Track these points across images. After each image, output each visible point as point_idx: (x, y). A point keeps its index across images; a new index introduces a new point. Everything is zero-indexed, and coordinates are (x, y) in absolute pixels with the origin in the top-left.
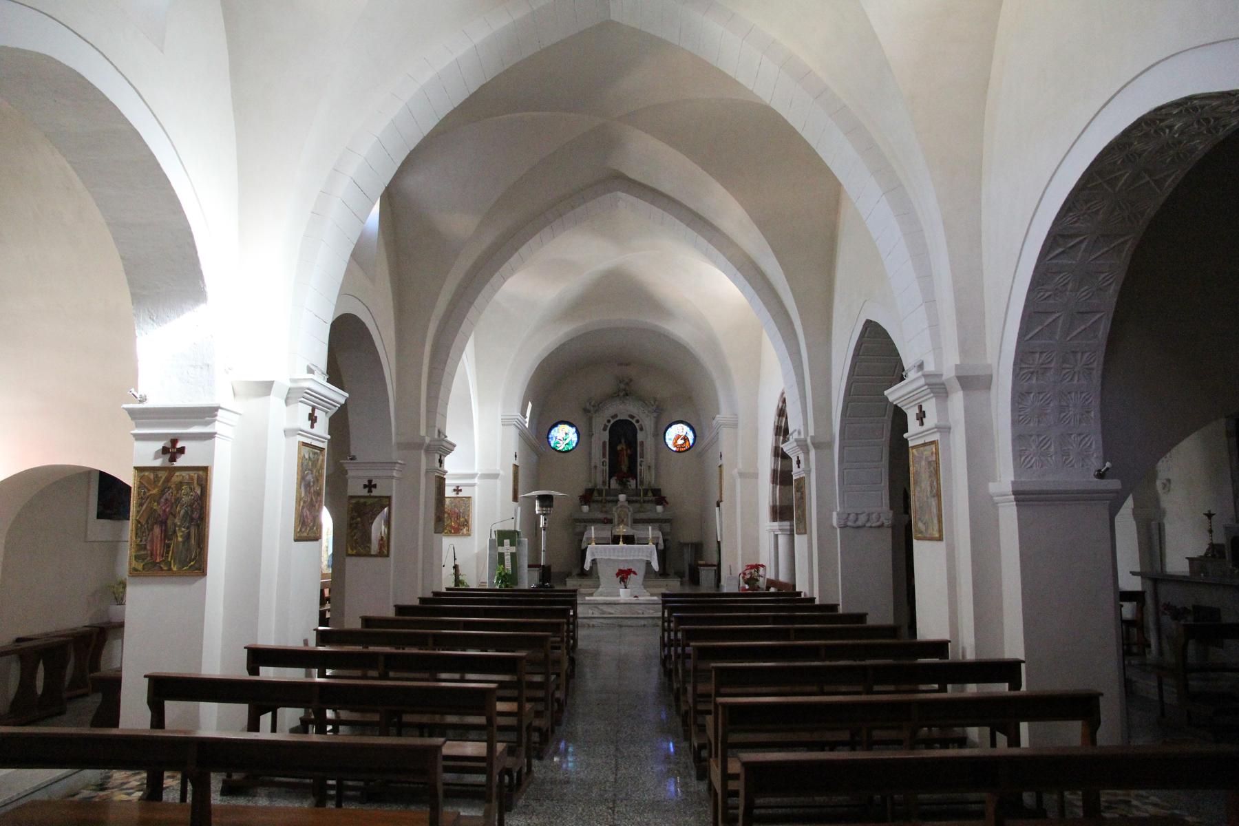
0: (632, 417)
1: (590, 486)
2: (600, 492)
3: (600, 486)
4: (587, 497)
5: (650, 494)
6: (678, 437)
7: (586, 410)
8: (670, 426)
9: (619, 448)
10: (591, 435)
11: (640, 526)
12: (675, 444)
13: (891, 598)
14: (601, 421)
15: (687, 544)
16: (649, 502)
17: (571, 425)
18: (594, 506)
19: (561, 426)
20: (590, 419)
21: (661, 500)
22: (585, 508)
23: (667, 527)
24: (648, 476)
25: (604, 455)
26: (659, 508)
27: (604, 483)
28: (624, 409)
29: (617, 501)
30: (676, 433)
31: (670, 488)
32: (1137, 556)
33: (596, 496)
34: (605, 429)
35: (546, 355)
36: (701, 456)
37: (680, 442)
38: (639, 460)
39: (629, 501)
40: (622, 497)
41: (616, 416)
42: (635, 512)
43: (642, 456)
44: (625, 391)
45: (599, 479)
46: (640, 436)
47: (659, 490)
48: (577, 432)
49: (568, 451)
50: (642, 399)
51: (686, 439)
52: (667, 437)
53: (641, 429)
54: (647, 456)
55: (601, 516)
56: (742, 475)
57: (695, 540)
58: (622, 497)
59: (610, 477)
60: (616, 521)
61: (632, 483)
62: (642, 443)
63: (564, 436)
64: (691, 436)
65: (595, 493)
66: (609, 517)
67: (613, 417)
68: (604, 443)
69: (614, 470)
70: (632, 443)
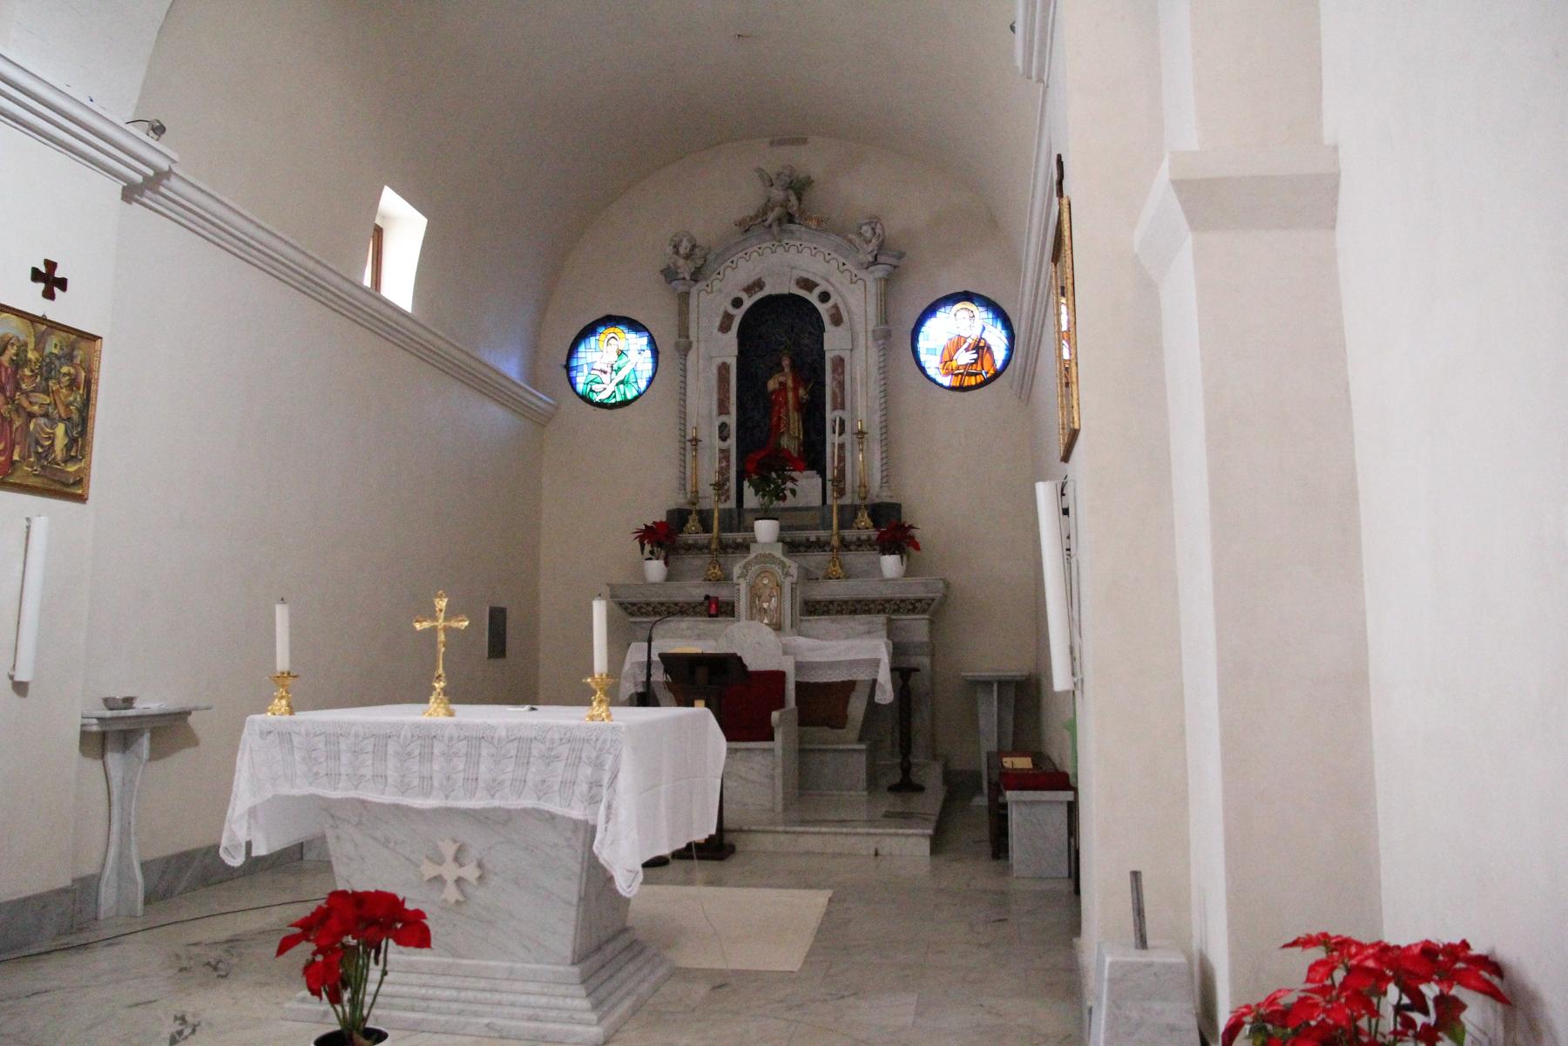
0: (808, 285)
3: (709, 500)
4: (662, 537)
5: (864, 520)
6: (957, 343)
7: (669, 274)
8: (931, 311)
10: (684, 349)
11: (822, 623)
12: (947, 360)
14: (715, 302)
15: (986, 684)
16: (860, 544)
18: (697, 562)
19: (605, 334)
20: (684, 298)
21: (893, 530)
22: (655, 569)
23: (917, 628)
24: (864, 468)
25: (723, 408)
26: (890, 564)
27: (720, 486)
28: (781, 266)
29: (1349, 970)
30: (952, 333)
31: (937, 497)
33: (692, 533)
34: (724, 328)
35: (1044, 701)
36: (1026, 390)
37: (964, 358)
39: (792, 547)
40: (765, 530)
41: (759, 284)
42: (808, 576)
43: (840, 405)
44: (790, 208)
46: (834, 341)
47: (896, 508)
48: (652, 342)
49: (625, 403)
50: (824, 226)
51: (981, 348)
52: (922, 345)
53: (837, 320)
54: (858, 399)
55: (694, 590)
56: (1207, 200)
57: (1014, 667)
58: (765, 530)
60: (742, 605)
61: (807, 488)
62: (839, 362)
63: (616, 362)
64: (997, 339)
65: (693, 524)
66: (723, 593)
67: (749, 290)
68: (723, 369)
70: (811, 368)
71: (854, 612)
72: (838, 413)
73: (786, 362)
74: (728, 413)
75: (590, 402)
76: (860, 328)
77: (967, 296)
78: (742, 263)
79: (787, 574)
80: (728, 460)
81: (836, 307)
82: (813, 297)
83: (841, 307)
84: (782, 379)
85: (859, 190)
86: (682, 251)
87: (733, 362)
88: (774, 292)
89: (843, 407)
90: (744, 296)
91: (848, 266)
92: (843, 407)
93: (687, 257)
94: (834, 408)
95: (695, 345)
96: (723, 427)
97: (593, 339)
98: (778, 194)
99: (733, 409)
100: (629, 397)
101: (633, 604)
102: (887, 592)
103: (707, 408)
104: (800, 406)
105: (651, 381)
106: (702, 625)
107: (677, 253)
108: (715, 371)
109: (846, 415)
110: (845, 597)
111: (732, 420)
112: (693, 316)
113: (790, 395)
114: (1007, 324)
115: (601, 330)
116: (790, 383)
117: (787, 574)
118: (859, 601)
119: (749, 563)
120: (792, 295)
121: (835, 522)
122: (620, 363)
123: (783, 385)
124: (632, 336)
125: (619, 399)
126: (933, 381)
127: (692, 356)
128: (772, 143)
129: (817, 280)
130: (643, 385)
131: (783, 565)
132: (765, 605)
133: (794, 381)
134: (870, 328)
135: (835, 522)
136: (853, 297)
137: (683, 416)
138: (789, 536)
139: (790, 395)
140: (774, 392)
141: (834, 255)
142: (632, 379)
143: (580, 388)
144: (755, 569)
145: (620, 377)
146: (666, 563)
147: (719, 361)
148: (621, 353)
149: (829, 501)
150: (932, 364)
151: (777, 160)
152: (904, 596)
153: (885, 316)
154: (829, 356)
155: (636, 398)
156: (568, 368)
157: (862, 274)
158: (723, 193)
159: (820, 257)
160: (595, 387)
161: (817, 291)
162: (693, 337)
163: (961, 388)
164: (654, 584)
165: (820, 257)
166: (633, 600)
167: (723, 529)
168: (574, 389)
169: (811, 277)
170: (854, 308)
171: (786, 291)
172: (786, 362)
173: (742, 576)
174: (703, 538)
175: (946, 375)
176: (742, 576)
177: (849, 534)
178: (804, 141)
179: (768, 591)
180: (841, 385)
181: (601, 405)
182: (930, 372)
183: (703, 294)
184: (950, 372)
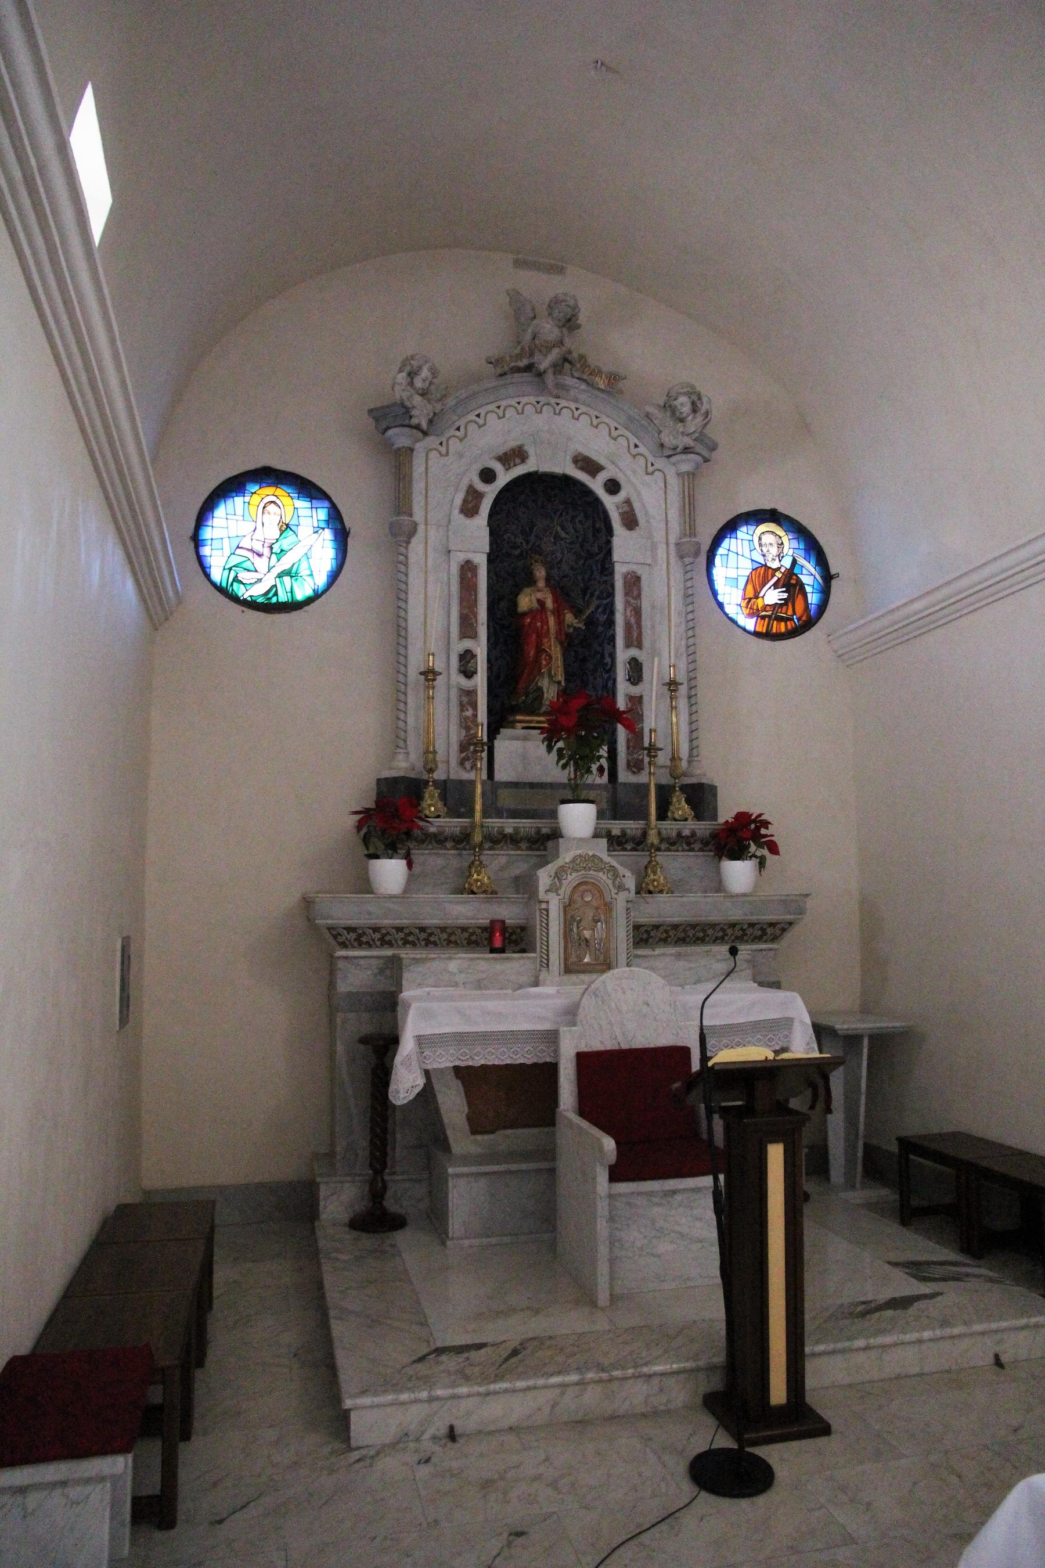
0: (592, 467)
1: (403, 766)
2: (457, 799)
3: (449, 767)
4: (392, 817)
5: (681, 807)
6: (762, 575)
9: (526, 601)
10: (400, 532)
12: (750, 601)
13: (74, 1258)
14: (449, 474)
16: (673, 843)
17: (307, 489)
18: (430, 859)
19: (258, 495)
20: (399, 463)
22: (390, 873)
25: (467, 628)
26: (739, 873)
27: (468, 747)
28: (559, 435)
32: (1014, 1141)
34: (469, 509)
37: (772, 596)
38: (622, 655)
43: (635, 640)
44: (544, 359)
45: (447, 736)
46: (626, 550)
48: (335, 518)
49: (292, 606)
51: (791, 583)
53: (631, 522)
55: (467, 912)
58: (578, 819)
59: (498, 722)
62: (634, 582)
63: (269, 543)
64: (809, 576)
65: (431, 803)
66: (509, 912)
68: (468, 569)
69: (509, 699)
71: (701, 940)
72: (633, 652)
73: (540, 573)
74: (474, 636)
75: (235, 599)
76: (659, 536)
77: (773, 516)
78: (492, 418)
79: (621, 888)
80: (474, 706)
81: (628, 502)
82: (596, 485)
83: (637, 506)
84: (539, 595)
85: (644, 349)
86: (418, 383)
87: (481, 561)
88: (546, 468)
89: (640, 646)
90: (498, 467)
91: (641, 449)
92: (640, 646)
93: (424, 394)
94: (628, 645)
95: (421, 528)
96: (467, 658)
97: (239, 500)
98: (549, 330)
99: (483, 632)
100: (300, 596)
101: (350, 929)
102: (736, 914)
103: (439, 621)
104: (570, 642)
105: (334, 577)
106: (483, 965)
107: (411, 384)
108: (455, 570)
109: (640, 655)
110: (676, 920)
111: (481, 649)
112: (418, 486)
113: (552, 621)
114: (822, 561)
115: (254, 488)
116: (549, 604)
117: (621, 888)
118: (693, 926)
119: (562, 869)
120: (567, 479)
121: (478, 807)
122: (285, 543)
123: (541, 603)
124: (303, 504)
125: (283, 597)
126: (734, 622)
127: (416, 546)
128: (518, 264)
129: (602, 461)
130: (321, 581)
131: (616, 875)
132: (587, 934)
133: (555, 600)
134: (672, 540)
135: (478, 807)
136: (647, 495)
137: (399, 631)
138: (616, 827)
139: (552, 621)
140: (530, 612)
141: (622, 431)
142: (304, 571)
143: (216, 575)
144: (572, 879)
145: (285, 564)
146: (410, 865)
147: (459, 558)
148: (285, 527)
149: (624, 776)
150: (733, 609)
151: (540, 287)
152: (754, 918)
153: (690, 528)
154: (620, 571)
155: (309, 601)
156: (197, 541)
157: (660, 463)
158: (455, 319)
159: (603, 430)
160: (243, 576)
161: (480, 486)
162: (418, 516)
163: (767, 635)
164: (391, 897)
165: (603, 430)
166: (353, 922)
167: (485, 814)
168: (207, 576)
169: (594, 457)
170: (652, 511)
171: (558, 470)
172: (540, 573)
173: (553, 889)
174: (453, 825)
175: (750, 615)
176: (553, 889)
177: (669, 827)
178: (561, 271)
179: (590, 914)
180: (637, 612)
181: (251, 605)
182: (731, 610)
183: (433, 455)
184: (754, 613)
